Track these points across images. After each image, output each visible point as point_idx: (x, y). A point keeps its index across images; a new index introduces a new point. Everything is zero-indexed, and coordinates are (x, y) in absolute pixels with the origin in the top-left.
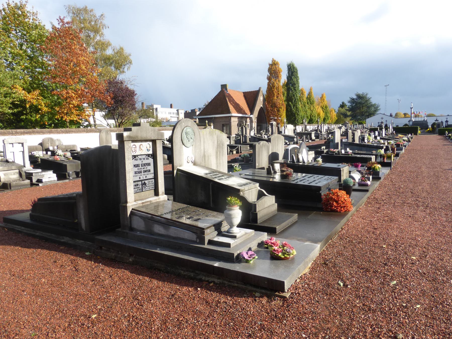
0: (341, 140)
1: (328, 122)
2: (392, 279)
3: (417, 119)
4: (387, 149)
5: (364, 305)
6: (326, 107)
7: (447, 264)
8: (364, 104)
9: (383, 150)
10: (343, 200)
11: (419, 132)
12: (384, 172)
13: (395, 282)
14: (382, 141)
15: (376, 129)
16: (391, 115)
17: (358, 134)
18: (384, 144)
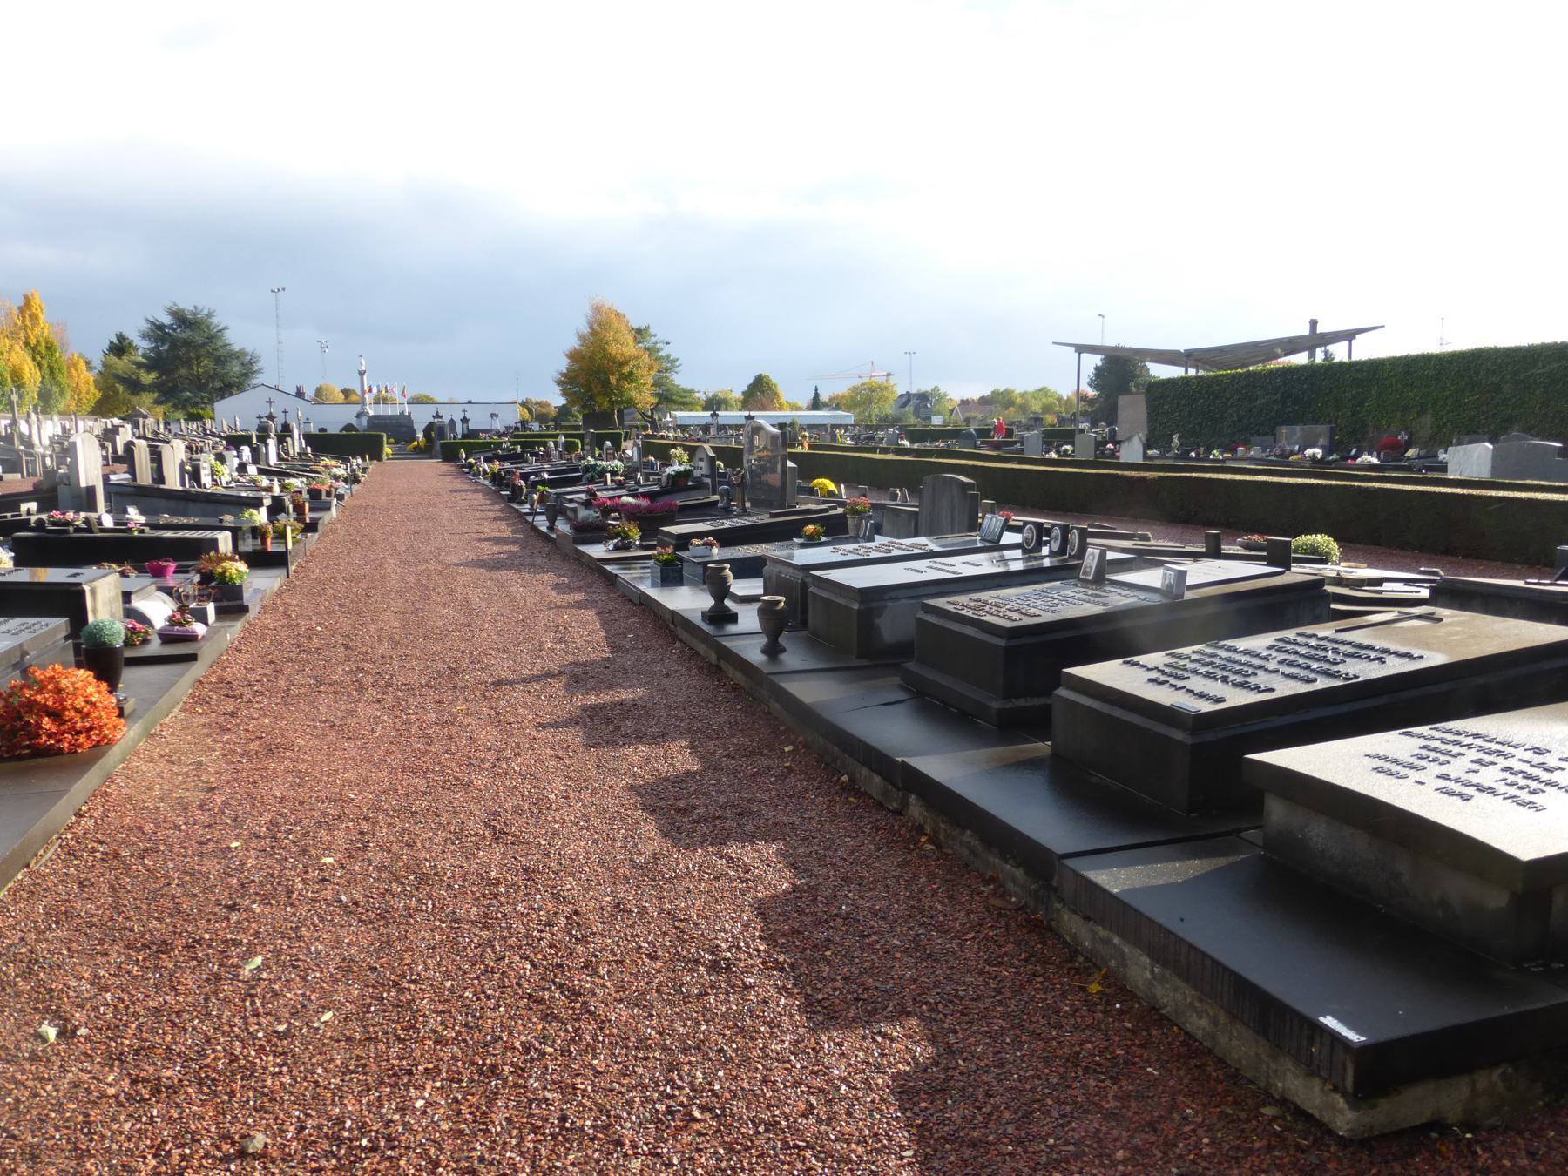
0: (106, 478)
1: (61, 407)
2: (250, 953)
3: (383, 410)
4: (277, 508)
5: (134, 1082)
6: (50, 348)
7: (424, 854)
8: (203, 345)
9: (263, 510)
10: (80, 703)
11: (387, 450)
12: (258, 585)
13: (258, 960)
14: (264, 481)
15: (246, 440)
16: (300, 394)
17: (175, 454)
18: (269, 489)
